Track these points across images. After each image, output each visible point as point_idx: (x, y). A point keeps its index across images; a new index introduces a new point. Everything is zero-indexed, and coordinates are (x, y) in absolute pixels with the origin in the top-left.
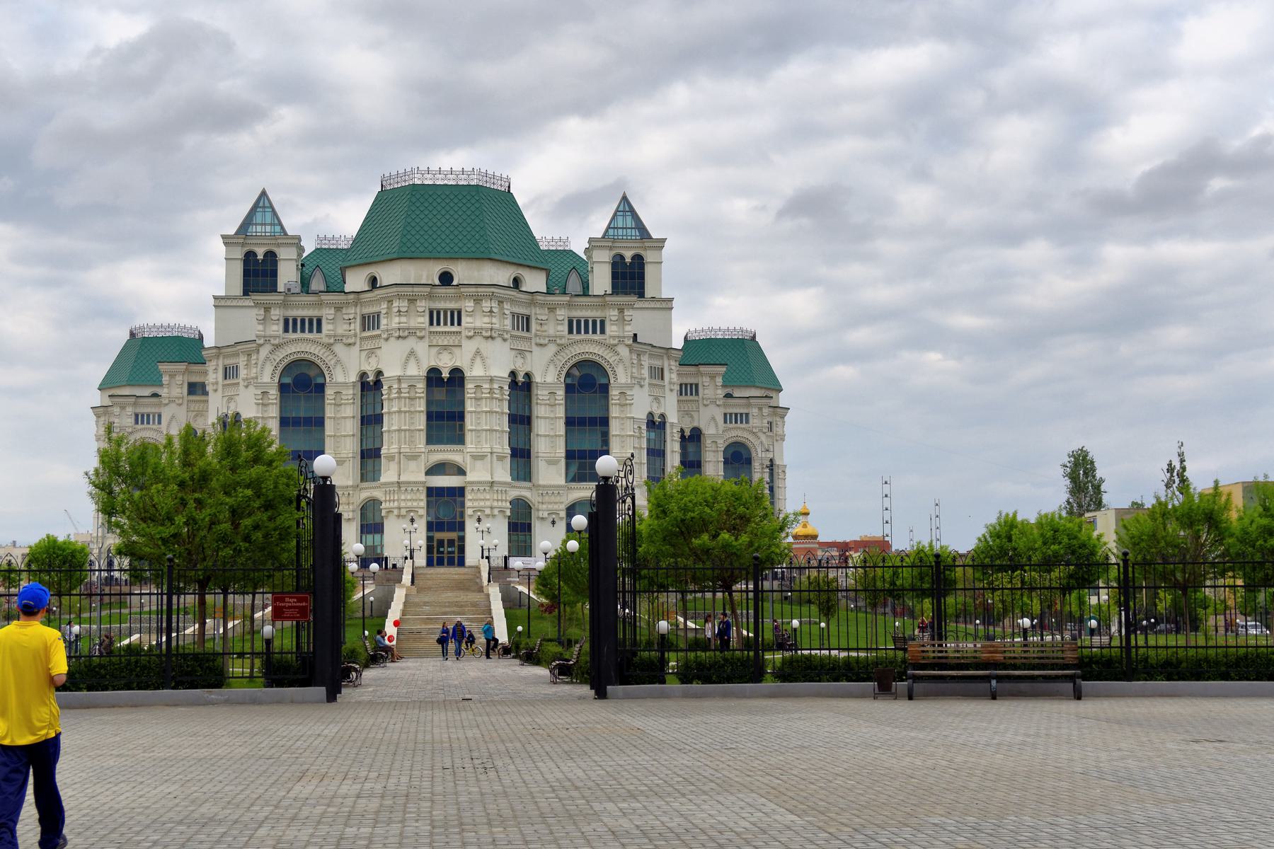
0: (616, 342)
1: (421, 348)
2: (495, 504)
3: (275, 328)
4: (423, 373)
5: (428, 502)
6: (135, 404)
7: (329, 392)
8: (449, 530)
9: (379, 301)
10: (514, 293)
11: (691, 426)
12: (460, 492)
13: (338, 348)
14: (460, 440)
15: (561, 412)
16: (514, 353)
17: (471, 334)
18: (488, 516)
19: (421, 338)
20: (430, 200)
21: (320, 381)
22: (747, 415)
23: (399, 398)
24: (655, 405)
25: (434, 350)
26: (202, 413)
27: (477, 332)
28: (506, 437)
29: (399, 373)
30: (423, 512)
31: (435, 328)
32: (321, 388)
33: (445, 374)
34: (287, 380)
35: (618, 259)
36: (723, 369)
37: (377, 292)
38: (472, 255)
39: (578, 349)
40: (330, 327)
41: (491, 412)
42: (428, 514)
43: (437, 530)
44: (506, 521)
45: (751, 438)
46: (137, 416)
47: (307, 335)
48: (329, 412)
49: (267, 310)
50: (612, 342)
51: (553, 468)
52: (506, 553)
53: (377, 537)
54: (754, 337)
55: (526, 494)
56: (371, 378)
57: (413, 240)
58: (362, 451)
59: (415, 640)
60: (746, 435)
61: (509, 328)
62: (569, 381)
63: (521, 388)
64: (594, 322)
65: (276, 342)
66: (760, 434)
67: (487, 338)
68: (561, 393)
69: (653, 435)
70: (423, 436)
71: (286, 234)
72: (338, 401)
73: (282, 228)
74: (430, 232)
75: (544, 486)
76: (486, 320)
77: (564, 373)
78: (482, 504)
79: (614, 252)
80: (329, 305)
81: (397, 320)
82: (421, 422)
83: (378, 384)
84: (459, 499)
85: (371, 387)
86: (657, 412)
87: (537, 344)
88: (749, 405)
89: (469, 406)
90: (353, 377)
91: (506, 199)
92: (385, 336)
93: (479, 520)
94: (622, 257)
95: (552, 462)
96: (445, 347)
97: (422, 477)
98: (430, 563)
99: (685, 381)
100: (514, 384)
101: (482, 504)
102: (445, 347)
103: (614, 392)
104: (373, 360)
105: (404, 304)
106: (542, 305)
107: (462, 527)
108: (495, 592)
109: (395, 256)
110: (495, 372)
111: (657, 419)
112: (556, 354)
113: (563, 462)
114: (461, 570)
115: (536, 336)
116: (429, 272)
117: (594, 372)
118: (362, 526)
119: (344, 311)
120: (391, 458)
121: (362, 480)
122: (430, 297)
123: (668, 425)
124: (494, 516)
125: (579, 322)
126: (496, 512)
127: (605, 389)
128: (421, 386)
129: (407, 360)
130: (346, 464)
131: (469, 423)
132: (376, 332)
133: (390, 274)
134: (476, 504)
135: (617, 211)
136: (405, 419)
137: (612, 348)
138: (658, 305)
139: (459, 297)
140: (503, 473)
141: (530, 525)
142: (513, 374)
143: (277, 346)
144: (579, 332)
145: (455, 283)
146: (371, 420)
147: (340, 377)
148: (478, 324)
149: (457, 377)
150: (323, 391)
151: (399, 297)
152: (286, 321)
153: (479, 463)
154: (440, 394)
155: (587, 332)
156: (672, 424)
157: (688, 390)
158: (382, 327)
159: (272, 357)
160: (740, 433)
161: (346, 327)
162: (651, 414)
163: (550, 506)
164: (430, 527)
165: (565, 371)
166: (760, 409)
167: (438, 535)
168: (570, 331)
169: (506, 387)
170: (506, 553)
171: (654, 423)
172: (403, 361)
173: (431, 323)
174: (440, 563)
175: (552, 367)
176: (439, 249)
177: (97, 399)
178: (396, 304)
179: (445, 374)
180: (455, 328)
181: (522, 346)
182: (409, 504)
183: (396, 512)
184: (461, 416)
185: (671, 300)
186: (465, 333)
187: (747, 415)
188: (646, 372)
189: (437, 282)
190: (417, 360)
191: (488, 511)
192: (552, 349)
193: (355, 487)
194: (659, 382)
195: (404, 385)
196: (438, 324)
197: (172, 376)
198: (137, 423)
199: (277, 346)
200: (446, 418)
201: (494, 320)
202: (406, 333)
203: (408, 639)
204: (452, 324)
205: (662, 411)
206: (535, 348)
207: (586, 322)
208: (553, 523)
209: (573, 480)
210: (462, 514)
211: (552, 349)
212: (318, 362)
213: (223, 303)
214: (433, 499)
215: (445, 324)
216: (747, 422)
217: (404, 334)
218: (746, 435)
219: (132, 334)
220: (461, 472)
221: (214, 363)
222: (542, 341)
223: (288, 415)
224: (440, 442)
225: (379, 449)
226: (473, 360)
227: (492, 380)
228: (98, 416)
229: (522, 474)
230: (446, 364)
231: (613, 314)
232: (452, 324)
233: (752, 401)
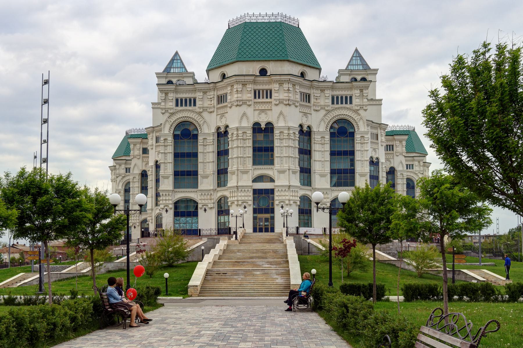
0: (359, 108)
1: (250, 111)
2: (291, 198)
3: (171, 104)
4: (251, 125)
5: (254, 198)
6: (126, 164)
7: (200, 138)
8: (265, 213)
9: (226, 87)
10: (301, 80)
11: (390, 166)
12: (272, 191)
13: (205, 115)
14: (272, 163)
15: (327, 147)
16: (301, 114)
17: (277, 103)
18: (287, 205)
19: (250, 105)
20: (255, 30)
21: (195, 133)
22: (412, 165)
23: (237, 139)
24: (374, 153)
25: (257, 112)
26: (147, 163)
27: (281, 102)
28: (297, 160)
29: (237, 125)
30: (251, 203)
31: (257, 100)
32: (196, 137)
33: (263, 126)
34: (178, 133)
36: (406, 137)
37: (225, 81)
38: (276, 59)
39: (337, 112)
40: (201, 103)
41: (289, 147)
42: (254, 204)
43: (259, 213)
44: (298, 207)
46: (126, 169)
47: (188, 108)
48: (200, 149)
49: (166, 94)
50: (356, 108)
51: (323, 179)
52: (298, 225)
53: (226, 217)
54: (414, 130)
55: (308, 193)
56: (222, 130)
57: (245, 51)
58: (218, 171)
59: (220, 280)
60: (412, 175)
61: (299, 100)
62: (332, 131)
63: (306, 133)
64: (346, 98)
65: (172, 111)
67: (286, 105)
68: (328, 137)
69: (372, 168)
70: (251, 160)
71: (187, 72)
72: (205, 143)
73: (186, 69)
74: (254, 47)
76: (286, 94)
77: (329, 126)
78: (284, 198)
79: (351, 77)
80: (200, 90)
81: (236, 96)
82: (250, 152)
83: (226, 132)
84: (271, 196)
85: (222, 135)
86: (375, 156)
87: (314, 110)
88: (413, 160)
89: (276, 143)
90: (213, 130)
91: (296, 32)
92: (230, 105)
93: (282, 207)
95: (322, 176)
96: (263, 111)
97: (250, 183)
98: (255, 230)
99: (389, 143)
100: (301, 132)
101: (284, 198)
102: (263, 111)
103: (357, 136)
104: (223, 120)
105: (239, 87)
106: (317, 88)
107: (272, 211)
108: (290, 244)
109: (235, 60)
110: (290, 124)
111: (374, 160)
113: (329, 175)
114: (272, 234)
115: (314, 105)
116: (254, 68)
117: (346, 126)
118: (218, 211)
119: (208, 94)
120: (233, 173)
121: (218, 186)
122: (254, 82)
123: (380, 164)
124: (290, 205)
125: (337, 98)
126: (292, 202)
127: (352, 134)
128: (250, 132)
129: (242, 118)
130: (210, 178)
131: (277, 153)
132: (225, 104)
133: (230, 71)
134: (280, 198)
135: (353, 56)
136: (241, 151)
138: (374, 103)
139: (270, 83)
140: (295, 180)
141: (310, 210)
142: (301, 126)
143: (172, 114)
144: (337, 103)
145: (268, 74)
146: (222, 153)
147: (206, 131)
148: (281, 97)
149: (270, 128)
150: (197, 138)
151: (237, 82)
152: (177, 100)
153: (282, 175)
154: (260, 137)
155: (342, 103)
156: (382, 163)
157: (389, 148)
158: (228, 101)
159: (169, 120)
161: (209, 103)
162: (371, 157)
164: (255, 211)
165: (330, 125)
166: (419, 162)
167: (259, 216)
168: (333, 103)
169: (297, 133)
170: (298, 225)
171: (373, 162)
172: (239, 119)
173: (255, 98)
174: (261, 230)
175: (322, 123)
176: (259, 56)
177: (112, 163)
178: (235, 87)
179: (263, 126)
180: (269, 100)
181: (306, 110)
182: (243, 198)
183: (236, 203)
184: (272, 149)
185: (381, 100)
186: (274, 102)
187: (412, 165)
189: (258, 74)
190: (247, 118)
191: (287, 202)
192: (323, 112)
193: (214, 190)
194: (376, 141)
195: (240, 132)
196: (259, 98)
197: (135, 145)
198: (127, 172)
199: (172, 114)
200: (263, 152)
201: (290, 95)
202: (241, 103)
203: (213, 280)
204: (267, 98)
205: (377, 156)
206: (313, 112)
207: (342, 98)
209: (335, 186)
210: (273, 204)
211: (323, 112)
212: (194, 122)
213: (156, 106)
214: (257, 196)
215: (263, 98)
216: (412, 168)
217: (241, 103)
218: (412, 175)
219: (127, 133)
220: (272, 180)
221: (151, 135)
222: (317, 108)
223: (179, 151)
224: (260, 164)
225: (227, 169)
226: (278, 117)
227: (289, 129)
228: (112, 170)
229: (306, 182)
230: (263, 120)
231: (357, 92)
232: (267, 98)
233: (415, 158)
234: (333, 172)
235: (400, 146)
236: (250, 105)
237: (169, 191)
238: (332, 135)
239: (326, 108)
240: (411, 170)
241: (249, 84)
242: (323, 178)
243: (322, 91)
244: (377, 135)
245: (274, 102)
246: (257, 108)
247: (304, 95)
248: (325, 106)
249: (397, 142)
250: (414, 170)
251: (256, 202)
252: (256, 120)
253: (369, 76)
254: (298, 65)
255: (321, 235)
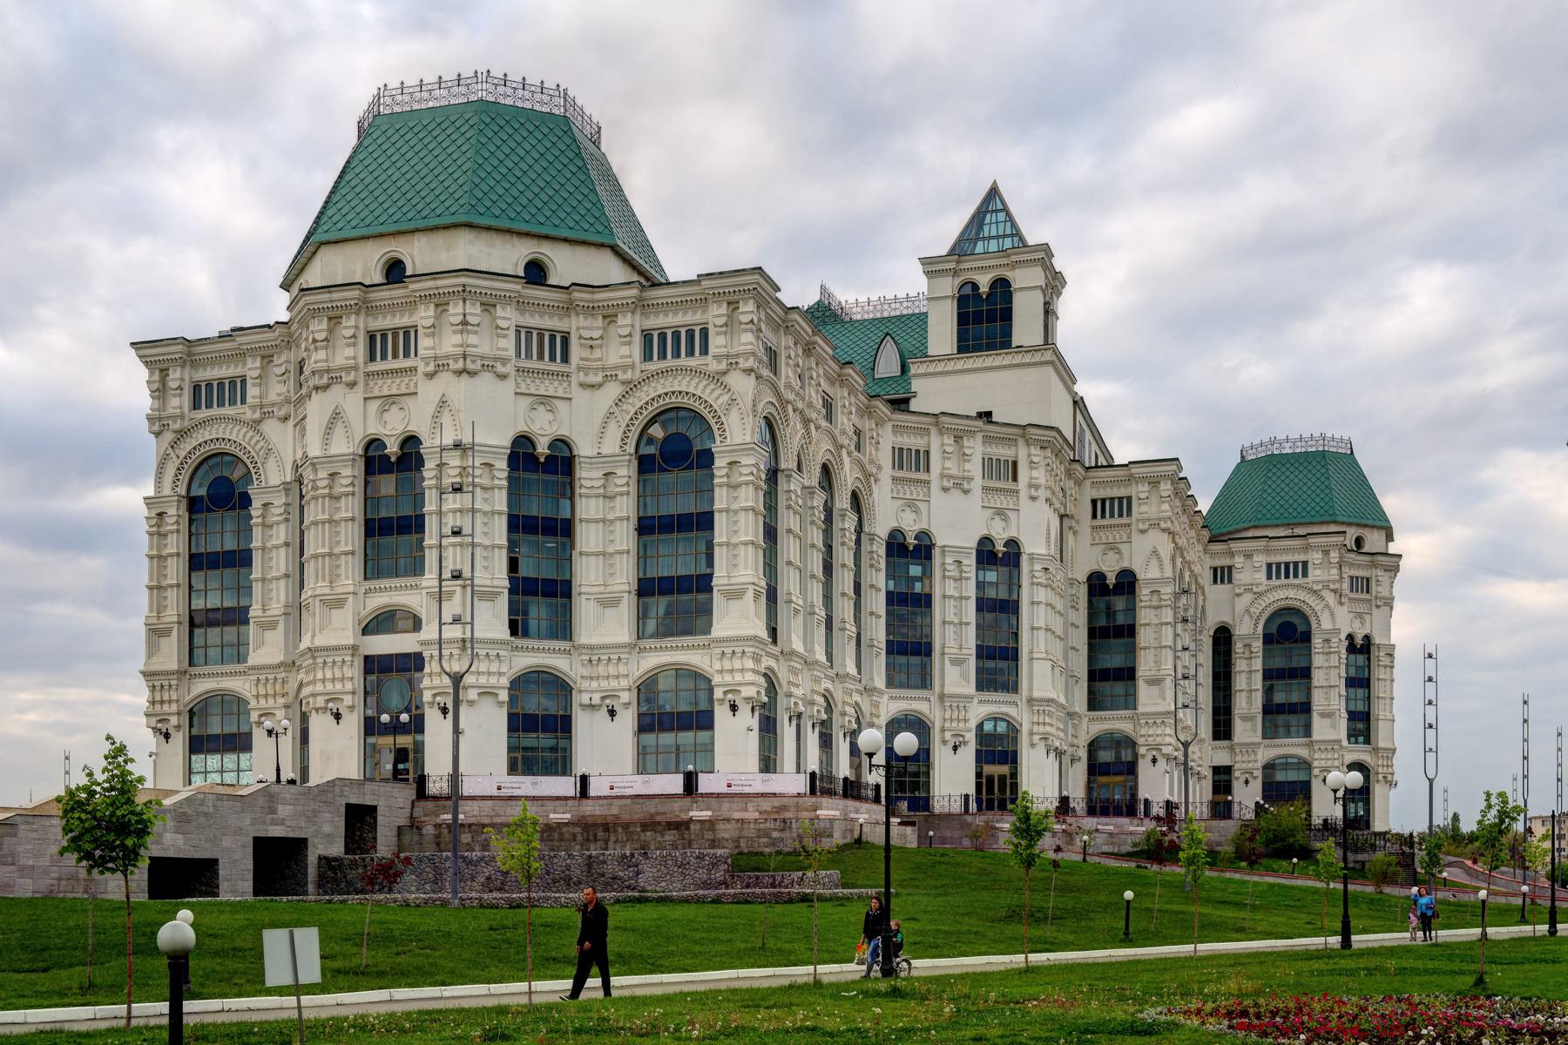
0: (723, 366)
1: (351, 403)
11: (1117, 568)
15: (500, 501)
19: (352, 385)
35: (968, 290)
45: (1310, 600)
60: (1302, 595)
63: (541, 469)
66: (1325, 593)
67: (459, 373)
75: (591, 647)
79: (958, 281)
87: (583, 385)
88: (1307, 548)
94: (975, 286)
102: (544, 400)
106: (591, 310)
112: (619, 402)
115: (579, 368)
122: (365, 307)
123: (1024, 559)
137: (717, 378)
149: (411, 454)
156: (1032, 557)
160: (1292, 593)
163: (604, 684)
166: (1326, 553)
167: (989, 769)
171: (993, 554)
179: (542, 449)
187: (1305, 564)
188: (975, 468)
200: (392, 535)
204: (541, 357)
206: (576, 392)
208: (612, 713)
211: (613, 390)
214: (373, 678)
216: (1305, 575)
218: (1302, 595)
233: (1312, 540)
234: (646, 588)
235: (1154, 499)
236: (352, 385)
237: (167, 673)
238: (645, 465)
239: (621, 376)
240: (1300, 581)
241: (349, 315)
242: (610, 612)
243: (610, 318)
244: (1015, 464)
245: (422, 368)
246: (377, 393)
247: (552, 338)
248: (496, 359)
249: (1141, 488)
250: (1311, 578)
251: (372, 700)
252: (374, 429)
253: (1018, 271)
254: (515, 239)
255: (566, 798)
